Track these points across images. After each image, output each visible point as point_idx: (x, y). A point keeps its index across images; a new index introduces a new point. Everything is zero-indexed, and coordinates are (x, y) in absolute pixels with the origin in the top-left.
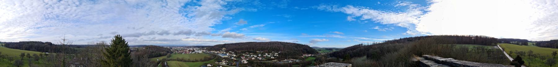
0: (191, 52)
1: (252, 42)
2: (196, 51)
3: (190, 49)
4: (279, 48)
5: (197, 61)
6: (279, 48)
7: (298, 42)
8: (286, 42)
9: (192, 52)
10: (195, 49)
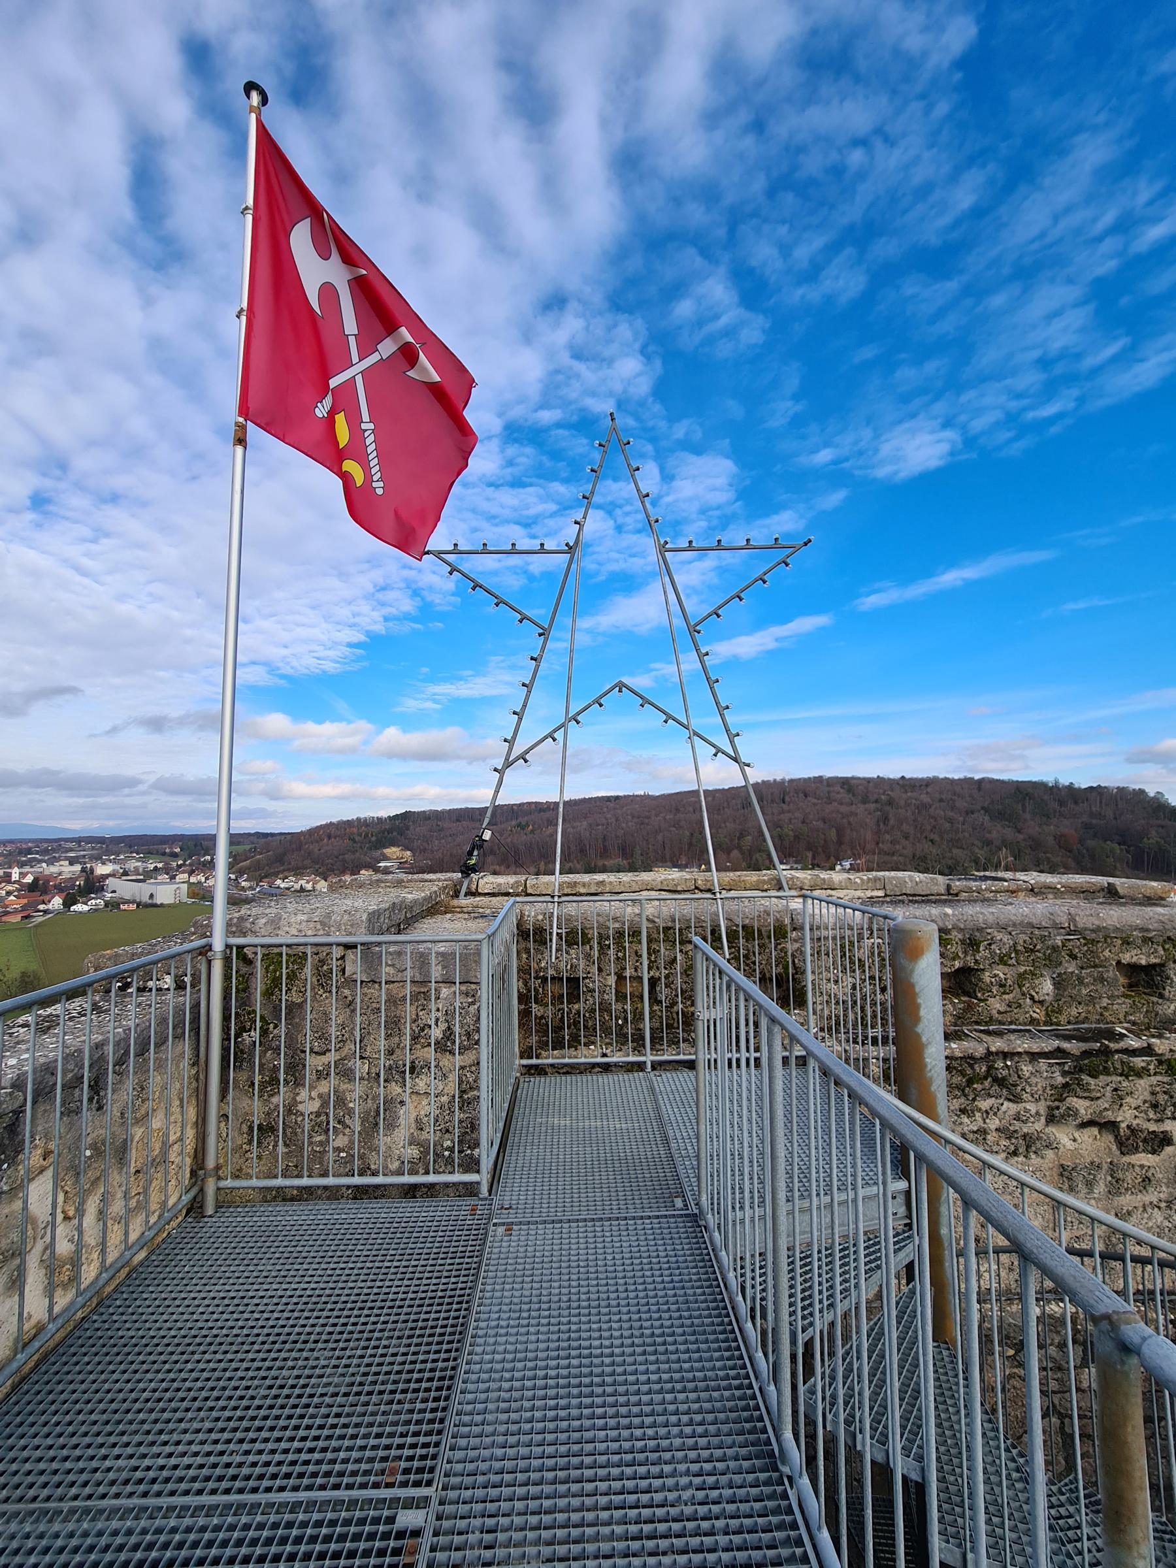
0: (57, 902)
1: (617, 798)
2: (123, 888)
3: (353, 857)
4: (840, 832)
5: (652, 889)
6: (840, 832)
7: (1002, 771)
8: (895, 775)
9: (69, 902)
10: (101, 870)
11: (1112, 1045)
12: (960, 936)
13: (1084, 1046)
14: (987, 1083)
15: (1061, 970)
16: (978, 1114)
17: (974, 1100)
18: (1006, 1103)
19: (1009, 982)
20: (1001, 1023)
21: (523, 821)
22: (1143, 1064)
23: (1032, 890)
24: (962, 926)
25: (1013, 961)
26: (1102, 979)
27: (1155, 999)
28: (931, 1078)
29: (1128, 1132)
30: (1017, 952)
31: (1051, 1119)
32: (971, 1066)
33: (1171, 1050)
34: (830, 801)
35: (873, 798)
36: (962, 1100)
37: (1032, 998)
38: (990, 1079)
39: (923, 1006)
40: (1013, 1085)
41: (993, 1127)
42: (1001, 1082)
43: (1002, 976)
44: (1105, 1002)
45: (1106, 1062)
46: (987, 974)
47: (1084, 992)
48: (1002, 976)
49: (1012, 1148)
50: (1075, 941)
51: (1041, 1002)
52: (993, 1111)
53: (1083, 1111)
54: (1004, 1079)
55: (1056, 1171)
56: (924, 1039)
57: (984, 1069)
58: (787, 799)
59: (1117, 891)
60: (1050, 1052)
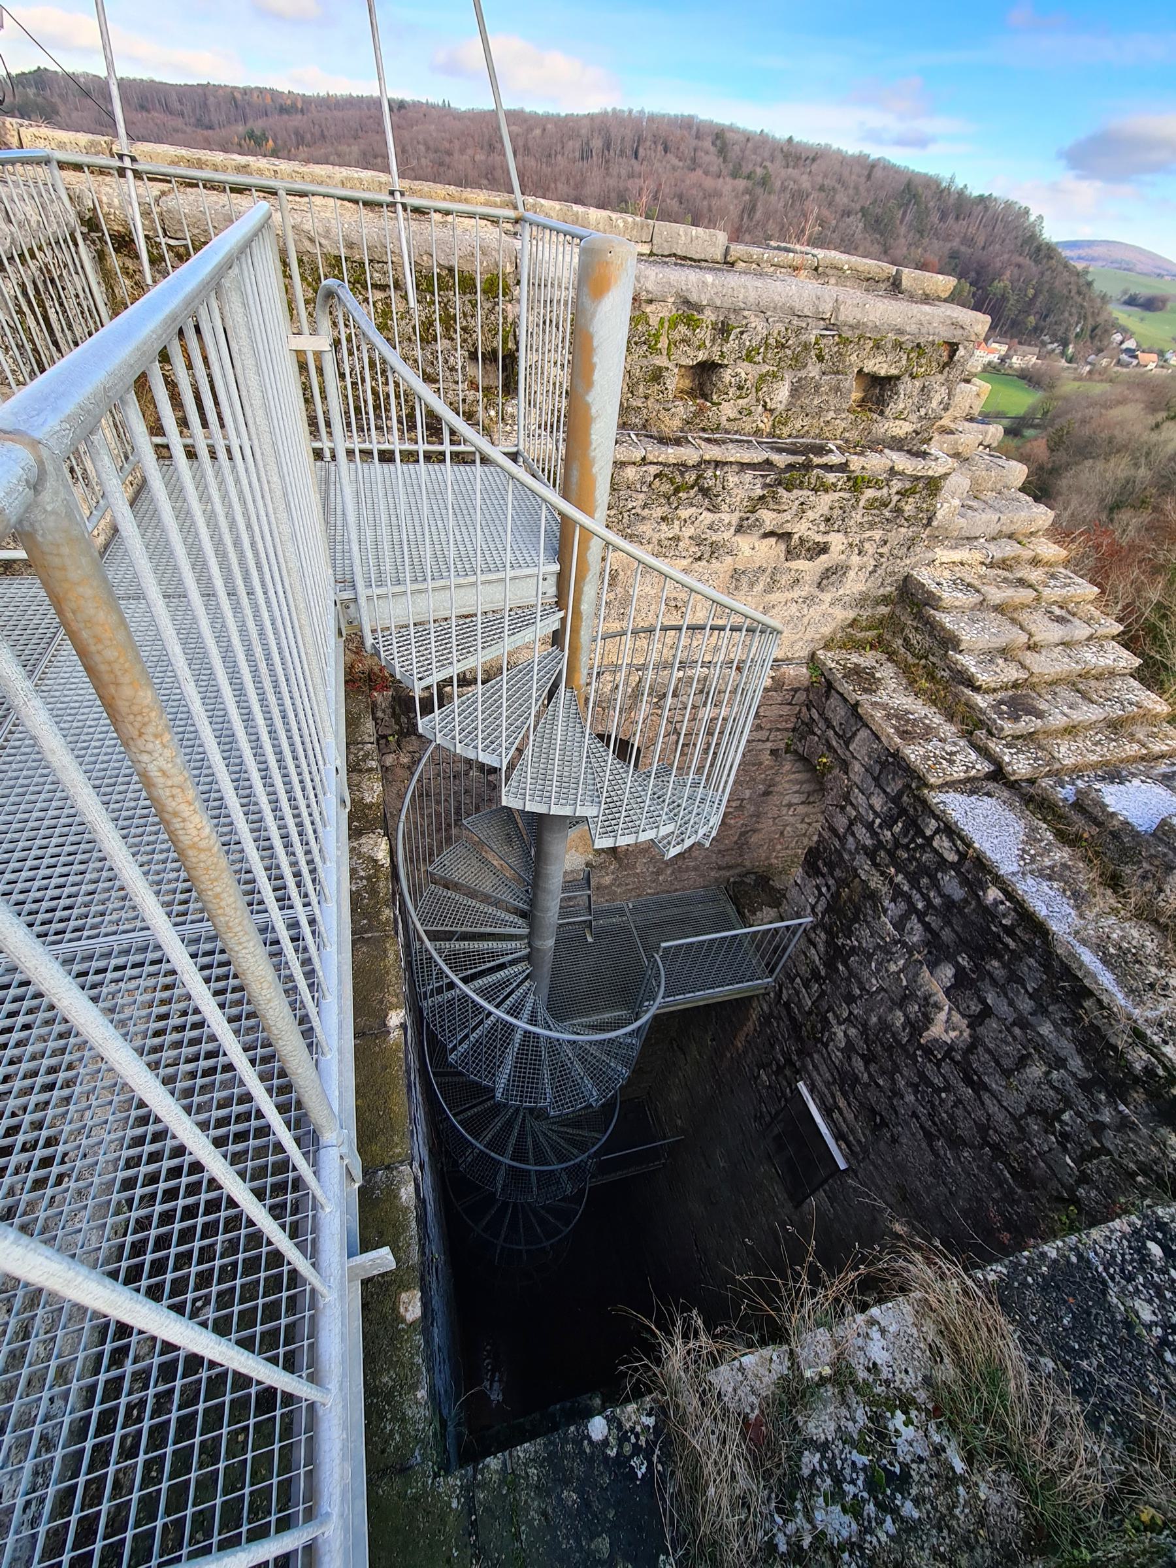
11: (815, 459)
12: (713, 318)
13: (791, 459)
14: (692, 493)
15: (803, 374)
16: (677, 522)
17: (676, 508)
18: (705, 513)
19: (749, 384)
20: (727, 432)
21: (258, 125)
22: (834, 480)
23: (816, 269)
24: (718, 304)
25: (759, 358)
26: (837, 389)
27: (875, 416)
28: (594, 458)
29: (798, 542)
30: (767, 345)
31: (739, 529)
32: (682, 474)
33: (863, 468)
34: (694, 165)
35: (746, 170)
36: (666, 508)
37: (764, 406)
38: (696, 488)
39: (598, 367)
40: (716, 496)
41: (687, 535)
42: (705, 492)
43: (743, 375)
44: (831, 414)
45: (804, 476)
46: (729, 371)
47: (816, 402)
48: (743, 375)
49: (699, 554)
50: (829, 345)
51: (772, 411)
52: (693, 520)
53: (768, 523)
54: (709, 489)
55: (729, 573)
56: (593, 411)
57: (694, 477)
58: (641, 152)
59: (900, 283)
60: (759, 463)
